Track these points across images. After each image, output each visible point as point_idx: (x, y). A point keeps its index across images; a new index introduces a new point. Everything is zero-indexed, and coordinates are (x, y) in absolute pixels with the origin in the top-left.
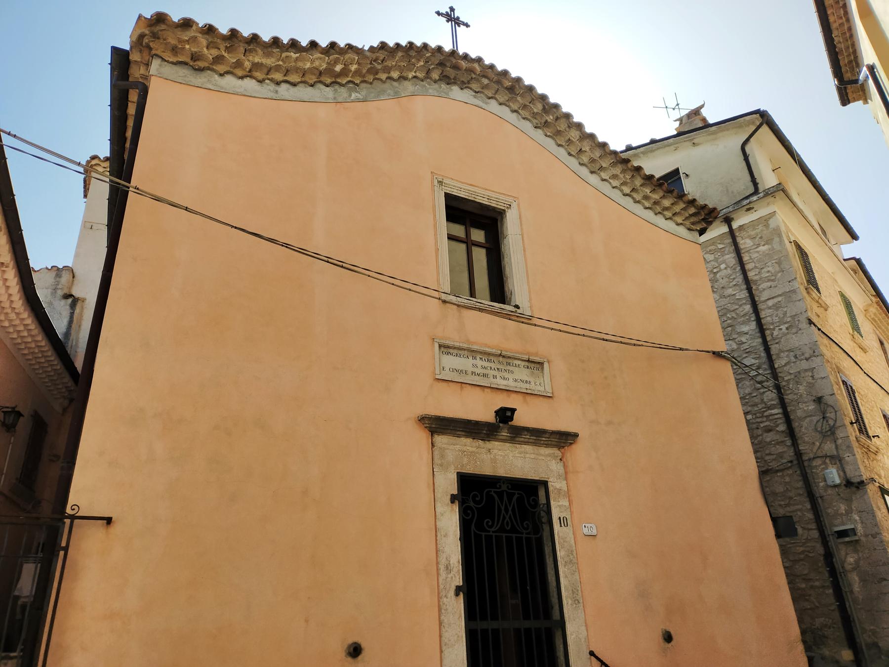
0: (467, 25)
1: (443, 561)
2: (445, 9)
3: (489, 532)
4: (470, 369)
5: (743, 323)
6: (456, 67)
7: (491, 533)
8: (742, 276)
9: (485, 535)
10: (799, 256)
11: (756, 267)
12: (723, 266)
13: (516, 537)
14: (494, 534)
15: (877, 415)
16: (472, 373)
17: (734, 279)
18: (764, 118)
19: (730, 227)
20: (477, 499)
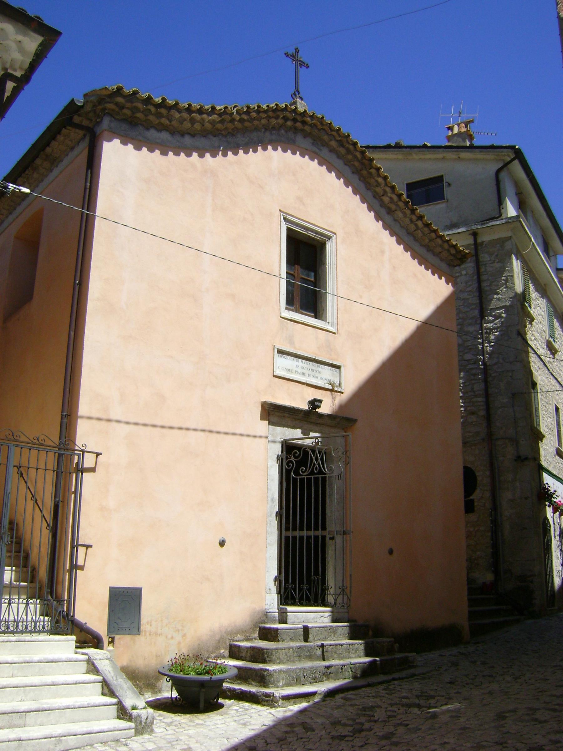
0: (307, 67)
1: (270, 495)
2: (291, 51)
3: (303, 475)
4: (295, 369)
5: (470, 324)
6: (304, 123)
7: (304, 477)
8: (477, 285)
9: (300, 478)
10: (521, 276)
11: (488, 279)
12: (464, 272)
13: (321, 477)
14: (305, 477)
15: (551, 408)
16: (296, 371)
17: (470, 285)
18: (518, 155)
19: (475, 240)
20: (296, 455)
